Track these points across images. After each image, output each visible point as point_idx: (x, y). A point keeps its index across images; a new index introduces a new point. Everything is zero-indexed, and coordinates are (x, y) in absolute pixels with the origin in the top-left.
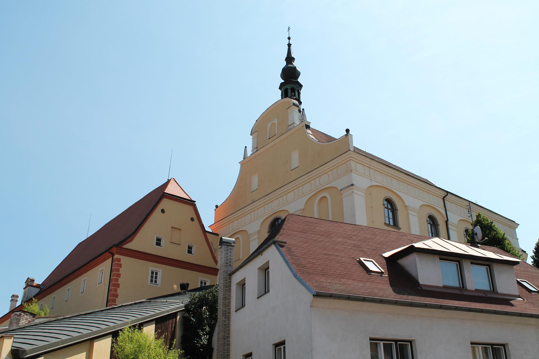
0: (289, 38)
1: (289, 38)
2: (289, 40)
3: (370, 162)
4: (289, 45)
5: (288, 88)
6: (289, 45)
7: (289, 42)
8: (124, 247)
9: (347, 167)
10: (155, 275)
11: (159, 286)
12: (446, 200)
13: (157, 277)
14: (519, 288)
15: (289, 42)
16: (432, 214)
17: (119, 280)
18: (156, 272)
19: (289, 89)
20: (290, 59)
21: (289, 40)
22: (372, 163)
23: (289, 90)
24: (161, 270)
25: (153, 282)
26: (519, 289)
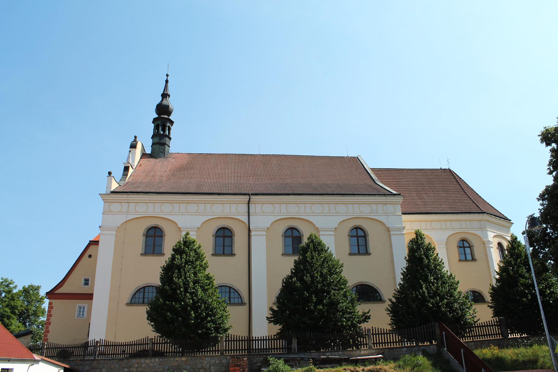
0: (167, 75)
1: (167, 75)
2: (167, 77)
3: (385, 199)
4: (167, 81)
5: (160, 124)
6: (167, 81)
7: (167, 78)
8: (55, 292)
9: (359, 208)
10: (83, 309)
11: (85, 318)
12: (323, 235)
13: (84, 314)
14: (101, 197)
15: (167, 78)
16: (225, 225)
17: (50, 320)
18: (83, 307)
19: (161, 125)
20: (165, 95)
21: (167, 77)
22: (388, 199)
23: (160, 126)
24: (87, 304)
25: (80, 316)
26: (103, 198)
